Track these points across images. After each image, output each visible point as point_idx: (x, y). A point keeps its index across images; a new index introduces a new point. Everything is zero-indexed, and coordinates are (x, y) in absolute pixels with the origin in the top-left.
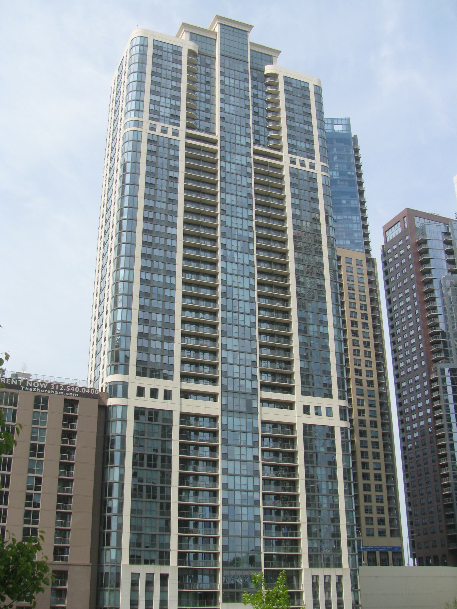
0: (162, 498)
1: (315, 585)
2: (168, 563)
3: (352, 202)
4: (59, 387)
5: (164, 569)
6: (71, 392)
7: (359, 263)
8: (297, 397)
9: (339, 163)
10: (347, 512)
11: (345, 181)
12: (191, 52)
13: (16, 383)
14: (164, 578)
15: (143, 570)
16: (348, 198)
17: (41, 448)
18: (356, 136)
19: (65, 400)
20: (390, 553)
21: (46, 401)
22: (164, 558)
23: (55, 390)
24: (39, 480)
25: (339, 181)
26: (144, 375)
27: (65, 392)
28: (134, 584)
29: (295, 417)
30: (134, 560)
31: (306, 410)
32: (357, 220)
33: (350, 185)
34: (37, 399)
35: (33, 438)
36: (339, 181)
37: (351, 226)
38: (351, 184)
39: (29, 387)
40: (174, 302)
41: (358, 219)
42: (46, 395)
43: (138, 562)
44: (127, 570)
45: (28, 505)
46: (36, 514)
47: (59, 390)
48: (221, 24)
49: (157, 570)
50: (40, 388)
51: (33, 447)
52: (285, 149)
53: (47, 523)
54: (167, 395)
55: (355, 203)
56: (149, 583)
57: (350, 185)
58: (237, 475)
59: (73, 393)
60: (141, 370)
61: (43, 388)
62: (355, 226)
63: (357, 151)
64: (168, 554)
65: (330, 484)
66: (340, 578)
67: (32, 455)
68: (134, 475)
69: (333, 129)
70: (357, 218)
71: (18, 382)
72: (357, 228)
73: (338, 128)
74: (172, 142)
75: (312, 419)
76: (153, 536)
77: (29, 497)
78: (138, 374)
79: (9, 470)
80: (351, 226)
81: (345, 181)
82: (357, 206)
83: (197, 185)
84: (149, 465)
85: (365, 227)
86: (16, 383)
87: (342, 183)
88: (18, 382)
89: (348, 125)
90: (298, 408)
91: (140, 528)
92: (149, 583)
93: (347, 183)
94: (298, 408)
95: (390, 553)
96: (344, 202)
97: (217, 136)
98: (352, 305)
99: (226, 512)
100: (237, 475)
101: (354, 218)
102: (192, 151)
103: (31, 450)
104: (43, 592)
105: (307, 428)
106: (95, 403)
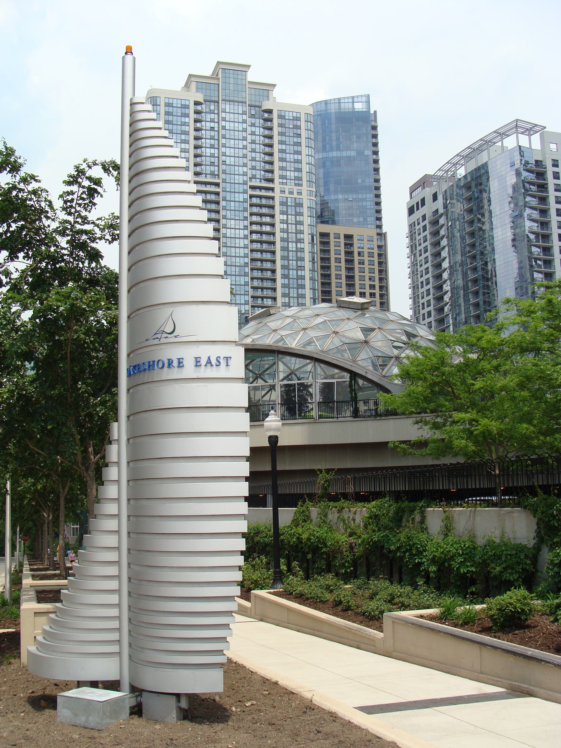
18: (375, 112)
37: (364, 204)
53: (459, 481)
55: (370, 181)
58: (233, 275)
62: (368, 203)
63: (375, 128)
69: (354, 108)
70: (371, 196)
72: (370, 205)
73: (359, 106)
74: (297, 201)
80: (364, 204)
83: (484, 638)
85: (378, 204)
89: (368, 102)
96: (360, 181)
98: (362, 278)
100: (233, 275)
101: (368, 196)
104: (64, 182)
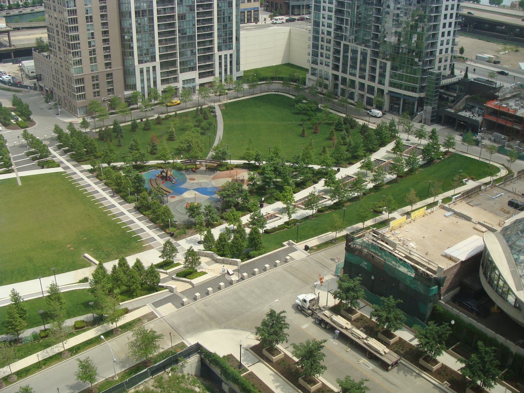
2: (155, 61)
5: (153, 64)
10: (236, 16)
14: (154, 68)
15: (144, 66)
17: (91, 17)
20: (253, 11)
22: (153, 59)
24: (92, 34)
28: (142, 72)
30: (140, 62)
43: (142, 63)
44: (138, 67)
45: (90, 47)
46: (94, 50)
49: (150, 65)
56: (148, 71)
64: (155, 57)
65: (229, 10)
66: (231, 55)
67: (91, 63)
68: (137, 21)
76: (148, 50)
77: (90, 43)
79: (81, 64)
91: (142, 47)
92: (148, 71)
95: (253, 11)
102: (167, 58)
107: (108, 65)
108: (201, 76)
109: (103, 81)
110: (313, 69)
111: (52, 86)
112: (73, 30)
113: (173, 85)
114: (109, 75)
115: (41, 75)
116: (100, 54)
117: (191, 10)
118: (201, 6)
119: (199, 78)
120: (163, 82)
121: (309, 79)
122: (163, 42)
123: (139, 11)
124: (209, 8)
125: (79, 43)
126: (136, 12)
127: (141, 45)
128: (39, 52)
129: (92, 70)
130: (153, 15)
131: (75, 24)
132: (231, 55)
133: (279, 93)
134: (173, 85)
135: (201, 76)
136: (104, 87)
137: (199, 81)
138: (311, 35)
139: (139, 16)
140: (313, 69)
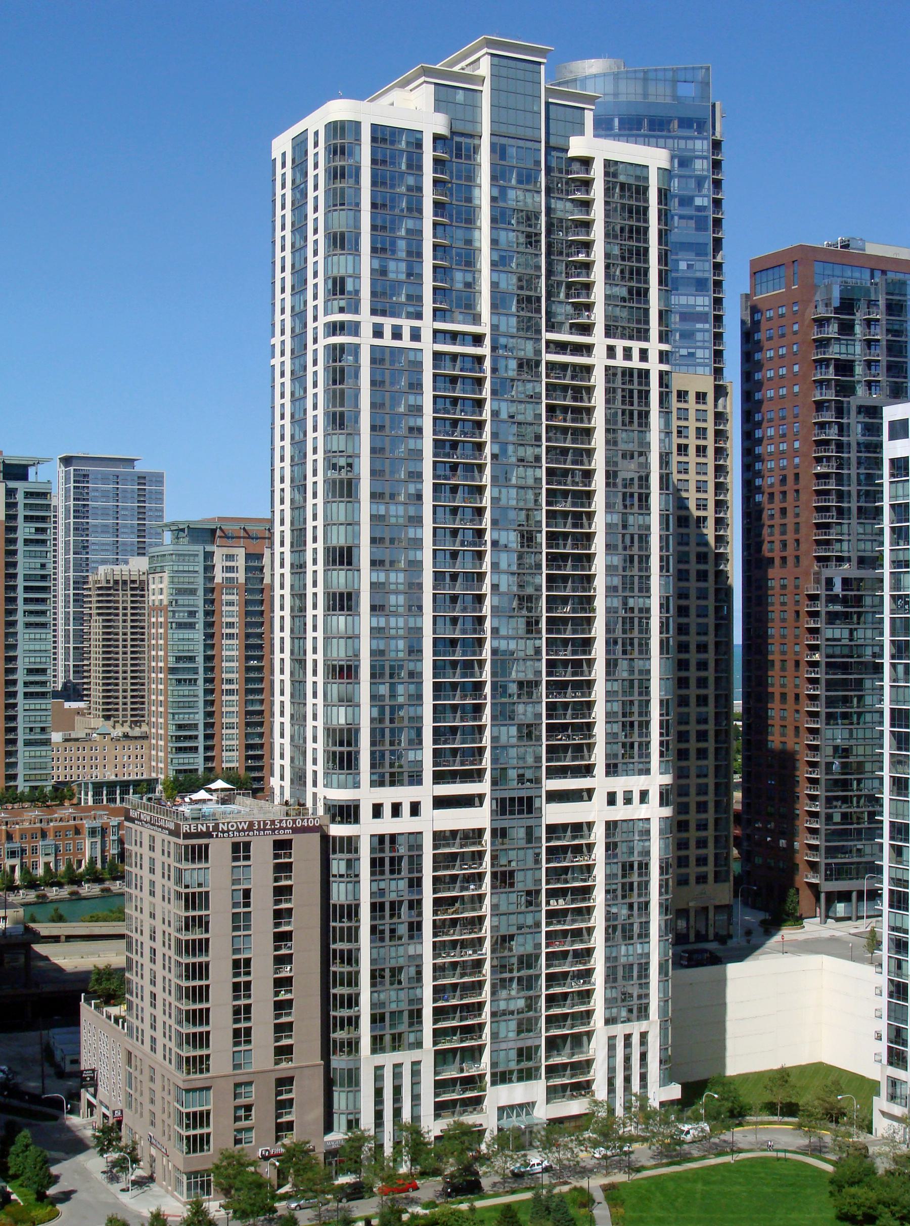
0: (411, 871)
1: (612, 1048)
3: (698, 266)
4: (265, 824)
6: (281, 828)
7: (701, 397)
8: (600, 782)
9: (680, 177)
11: (690, 218)
12: (437, 138)
13: (204, 829)
16: (691, 256)
17: (248, 962)
19: (275, 842)
21: (247, 845)
23: (259, 830)
24: (247, 893)
25: (676, 218)
26: (381, 784)
27: (273, 830)
29: (594, 812)
31: (611, 799)
32: (704, 341)
33: (698, 229)
34: (236, 847)
35: (236, 951)
36: (676, 218)
38: (701, 224)
39: (223, 832)
40: (421, 548)
41: (707, 339)
42: (247, 839)
47: (264, 830)
48: (492, 55)
50: (239, 831)
51: (236, 964)
52: (599, 329)
54: (415, 809)
57: (698, 229)
59: (284, 829)
60: (375, 777)
61: (243, 830)
66: (644, 1036)
71: (208, 827)
75: (620, 812)
78: (373, 784)
81: (690, 218)
82: (706, 275)
84: (392, 872)
86: (204, 829)
87: (684, 222)
88: (208, 827)
90: (600, 797)
93: (692, 223)
94: (600, 797)
97: (485, 328)
99: (496, 603)
103: (234, 1037)
105: (611, 826)
106: (316, 837)
107: (284, 1052)
108: (553, 1093)
109: (262, 1097)
110: (894, 1083)
111: (120, 1105)
112: (194, 926)
113: (470, 1119)
114: (285, 1082)
115: (93, 1071)
116: (262, 1020)
117: (529, 903)
118: (563, 893)
119: (548, 1101)
120: (440, 1108)
121: (883, 1113)
122: (447, 450)
123: (382, 905)
124: (584, 900)
125: (208, 1056)
126: (373, 906)
127: (382, 512)
128: (97, 1007)
129: (236, 1066)
130: (420, 870)
131: (201, 979)
132: (644, 1036)
133: (789, 1155)
134: (470, 1119)
135: (553, 1093)
136: (263, 1117)
137: (543, 1112)
138: (882, 1026)
139: (382, 873)
140: (894, 1083)
